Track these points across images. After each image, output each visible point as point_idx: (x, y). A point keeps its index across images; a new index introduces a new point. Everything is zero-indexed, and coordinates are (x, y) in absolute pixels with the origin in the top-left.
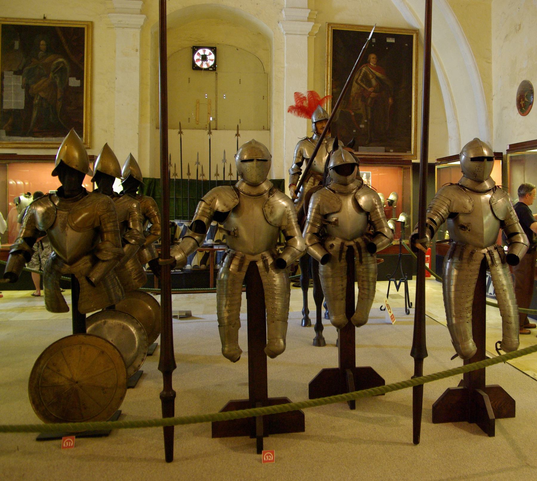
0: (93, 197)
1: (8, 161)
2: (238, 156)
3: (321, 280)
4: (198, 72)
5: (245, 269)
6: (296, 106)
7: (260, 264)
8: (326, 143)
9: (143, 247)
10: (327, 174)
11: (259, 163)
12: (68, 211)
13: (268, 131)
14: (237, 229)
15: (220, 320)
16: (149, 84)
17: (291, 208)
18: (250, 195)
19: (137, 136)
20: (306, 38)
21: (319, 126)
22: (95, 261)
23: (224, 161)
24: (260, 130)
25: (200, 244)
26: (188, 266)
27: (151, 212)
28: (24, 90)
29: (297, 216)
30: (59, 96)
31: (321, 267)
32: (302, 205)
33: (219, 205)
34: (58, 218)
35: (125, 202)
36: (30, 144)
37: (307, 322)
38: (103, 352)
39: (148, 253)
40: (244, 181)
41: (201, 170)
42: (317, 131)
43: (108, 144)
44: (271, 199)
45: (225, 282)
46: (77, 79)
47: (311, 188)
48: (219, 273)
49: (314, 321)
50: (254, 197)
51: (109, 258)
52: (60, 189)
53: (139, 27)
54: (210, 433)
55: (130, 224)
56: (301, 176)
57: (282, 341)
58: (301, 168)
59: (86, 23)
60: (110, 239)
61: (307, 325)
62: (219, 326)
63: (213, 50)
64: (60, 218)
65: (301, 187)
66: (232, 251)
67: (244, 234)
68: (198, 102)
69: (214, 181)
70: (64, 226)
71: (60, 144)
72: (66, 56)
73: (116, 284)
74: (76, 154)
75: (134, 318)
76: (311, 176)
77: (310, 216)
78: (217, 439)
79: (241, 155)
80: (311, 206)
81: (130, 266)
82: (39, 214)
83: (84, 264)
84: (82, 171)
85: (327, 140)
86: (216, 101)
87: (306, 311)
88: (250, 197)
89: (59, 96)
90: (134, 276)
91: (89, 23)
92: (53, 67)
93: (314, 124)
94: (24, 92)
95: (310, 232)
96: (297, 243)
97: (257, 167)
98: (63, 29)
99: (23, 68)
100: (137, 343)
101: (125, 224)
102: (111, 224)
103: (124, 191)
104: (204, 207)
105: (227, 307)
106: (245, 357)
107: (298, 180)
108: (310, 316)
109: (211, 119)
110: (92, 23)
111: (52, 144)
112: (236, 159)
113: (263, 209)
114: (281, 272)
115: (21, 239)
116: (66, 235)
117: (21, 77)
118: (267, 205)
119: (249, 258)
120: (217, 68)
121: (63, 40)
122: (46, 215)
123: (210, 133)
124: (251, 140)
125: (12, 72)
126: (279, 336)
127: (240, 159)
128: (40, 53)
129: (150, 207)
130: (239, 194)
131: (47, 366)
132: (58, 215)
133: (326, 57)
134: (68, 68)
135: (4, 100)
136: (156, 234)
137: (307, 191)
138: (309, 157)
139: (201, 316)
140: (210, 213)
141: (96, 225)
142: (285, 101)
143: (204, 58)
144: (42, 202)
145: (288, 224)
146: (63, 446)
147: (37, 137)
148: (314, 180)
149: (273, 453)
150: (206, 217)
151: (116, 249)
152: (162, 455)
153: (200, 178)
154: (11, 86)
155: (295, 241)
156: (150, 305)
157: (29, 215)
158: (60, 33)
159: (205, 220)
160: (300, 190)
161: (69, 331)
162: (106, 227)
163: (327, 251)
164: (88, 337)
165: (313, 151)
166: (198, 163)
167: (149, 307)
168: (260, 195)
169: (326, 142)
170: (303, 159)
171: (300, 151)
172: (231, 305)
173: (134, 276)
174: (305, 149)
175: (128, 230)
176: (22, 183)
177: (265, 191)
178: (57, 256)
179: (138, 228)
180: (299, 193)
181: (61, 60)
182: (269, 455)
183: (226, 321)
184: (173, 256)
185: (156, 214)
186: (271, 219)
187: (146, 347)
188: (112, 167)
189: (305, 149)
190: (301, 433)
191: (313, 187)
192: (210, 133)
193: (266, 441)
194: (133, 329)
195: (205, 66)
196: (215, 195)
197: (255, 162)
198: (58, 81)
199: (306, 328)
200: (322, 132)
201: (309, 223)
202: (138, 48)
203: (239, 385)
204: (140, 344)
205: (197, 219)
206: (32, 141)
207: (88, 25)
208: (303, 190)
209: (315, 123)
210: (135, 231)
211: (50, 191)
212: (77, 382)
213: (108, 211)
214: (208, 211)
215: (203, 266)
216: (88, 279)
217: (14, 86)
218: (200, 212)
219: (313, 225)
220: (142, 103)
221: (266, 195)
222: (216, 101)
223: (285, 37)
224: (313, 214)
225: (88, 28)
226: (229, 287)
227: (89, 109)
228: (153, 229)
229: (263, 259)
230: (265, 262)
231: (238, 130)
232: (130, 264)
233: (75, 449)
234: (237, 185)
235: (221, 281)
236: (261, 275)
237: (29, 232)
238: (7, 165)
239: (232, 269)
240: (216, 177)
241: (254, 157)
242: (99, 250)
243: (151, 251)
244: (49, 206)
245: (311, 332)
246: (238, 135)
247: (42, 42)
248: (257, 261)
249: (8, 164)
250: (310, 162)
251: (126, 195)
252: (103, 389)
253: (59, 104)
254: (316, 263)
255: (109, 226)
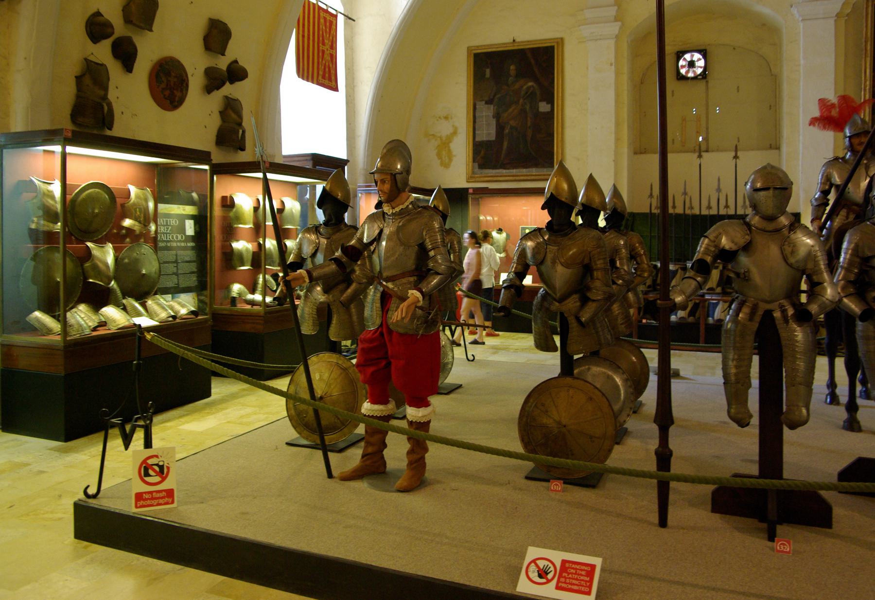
0: (583, 231)
1: (481, 195)
2: (749, 184)
3: (860, 342)
4: (683, 82)
5: (758, 318)
6: (821, 116)
7: (777, 314)
8: (866, 164)
9: (628, 291)
10: (869, 203)
11: (777, 192)
12: (558, 246)
13: (777, 151)
14: (748, 271)
15: (726, 376)
16: (626, 102)
17: (819, 247)
18: (764, 231)
19: (613, 163)
20: (831, 22)
21: (856, 141)
22: (585, 300)
23: (719, 190)
24: (766, 149)
25: (703, 287)
26: (673, 318)
27: (637, 251)
28: (495, 120)
29: (826, 258)
30: (529, 124)
31: (860, 325)
32: (829, 245)
33: (725, 242)
34: (548, 253)
35: (612, 238)
36: (501, 176)
37: (834, 399)
38: (591, 399)
39: (633, 297)
40: (756, 214)
41: (689, 202)
42: (852, 148)
43: (593, 174)
44: (793, 236)
45: (732, 333)
46: (548, 103)
47: (843, 223)
48: (724, 322)
49: (844, 398)
50: (769, 233)
51: (599, 298)
52: (549, 223)
53: (614, 37)
54: (709, 507)
55: (616, 263)
56: (828, 208)
57: (804, 411)
58: (829, 197)
59: (556, 41)
60: (600, 277)
61: (834, 403)
62: (724, 383)
63: (681, 55)
64: (550, 253)
65: (829, 223)
66: (741, 297)
67: (756, 277)
68: (684, 120)
69: (705, 216)
70: (554, 263)
71: (550, 175)
72: (536, 80)
73: (606, 327)
74: (565, 186)
75: (619, 367)
76: (843, 207)
77: (844, 258)
78: (718, 516)
79: (753, 182)
80: (845, 245)
81: (616, 309)
82: (529, 248)
83: (572, 303)
84: (571, 204)
85: (867, 159)
86: (707, 117)
87: (832, 384)
88: (765, 233)
89: (529, 124)
90: (620, 321)
91: (559, 40)
92: (523, 93)
93: (848, 139)
94: (495, 122)
95: (844, 278)
96: (826, 291)
97: (774, 196)
98: (533, 50)
99: (494, 96)
100: (622, 395)
101: (612, 262)
102: (601, 261)
103: (607, 226)
104: (708, 245)
105: (735, 362)
106: (755, 421)
107: (823, 214)
108: (838, 391)
109: (701, 139)
110: (562, 39)
111: (522, 176)
112: (746, 187)
113: (781, 248)
114: (805, 326)
115: (512, 273)
116: (556, 271)
117: (492, 107)
118: (786, 243)
119: (763, 307)
120: (707, 75)
121: (533, 61)
122: (536, 250)
123: (700, 156)
124: (764, 164)
125: (484, 102)
126: (801, 404)
127: (751, 187)
128: (510, 78)
129: (635, 244)
130: (750, 229)
131: (535, 405)
132: (548, 250)
133: (864, 44)
134: (538, 93)
135: (477, 132)
136: (642, 275)
137: (837, 228)
138: (839, 183)
139: (692, 377)
140: (714, 251)
141: (586, 261)
142: (801, 109)
143: (691, 64)
144: (532, 237)
145: (815, 267)
146: (551, 488)
147: (508, 169)
148: (848, 214)
149: (789, 543)
150: (709, 255)
151: (606, 289)
152: (655, 518)
153: (688, 212)
154: (483, 116)
155: (825, 289)
156: (634, 356)
157: (520, 249)
158: (529, 55)
159: (709, 259)
160: (827, 226)
161: (556, 371)
162: (596, 264)
163: (867, 303)
164: (576, 380)
165: (846, 175)
166: (685, 193)
167: (634, 358)
168: (778, 231)
169: (865, 162)
170: (831, 185)
171: (827, 176)
172: (739, 360)
173: (620, 321)
174: (834, 173)
175: (614, 270)
176: (491, 218)
177: (785, 226)
178: (546, 292)
179: (626, 268)
180: (825, 230)
181: (530, 84)
182: (784, 544)
183: (733, 378)
184: (673, 298)
185: (642, 253)
186: (792, 260)
187: (632, 401)
188: (597, 199)
189: (834, 173)
190: (828, 530)
191: (846, 222)
192: (700, 156)
193: (780, 529)
194: (618, 380)
195: (691, 75)
196: (721, 231)
197: (771, 191)
198: (528, 107)
199: (832, 406)
200: (861, 148)
201: (842, 267)
202: (613, 61)
203: (742, 460)
204: (625, 398)
205: (699, 257)
206: (503, 173)
207: (557, 43)
208: (831, 225)
209: (850, 137)
210: (622, 271)
211: (521, 227)
212: (565, 426)
213: (599, 247)
214: (713, 249)
215: (691, 319)
216: (578, 319)
217: (486, 116)
218: (702, 249)
219: (848, 270)
220: (618, 124)
221: (785, 231)
222: (707, 117)
223: (801, 25)
224: (848, 256)
225: (558, 46)
226: (738, 339)
227: (560, 136)
228: (640, 270)
229: (781, 308)
230: (784, 312)
231: (736, 151)
232: (616, 308)
233: (563, 494)
234: (748, 220)
235: (727, 331)
236: (778, 327)
237: (520, 267)
238: (480, 199)
239: (742, 318)
240: (707, 211)
241: (770, 185)
242: (589, 289)
243: (636, 294)
244: (539, 241)
245: (841, 414)
246: (736, 157)
247: (512, 67)
248: (774, 311)
249: (481, 198)
250: (842, 190)
251: (612, 231)
252: (591, 437)
253: (530, 133)
254: (850, 318)
255: (600, 264)
